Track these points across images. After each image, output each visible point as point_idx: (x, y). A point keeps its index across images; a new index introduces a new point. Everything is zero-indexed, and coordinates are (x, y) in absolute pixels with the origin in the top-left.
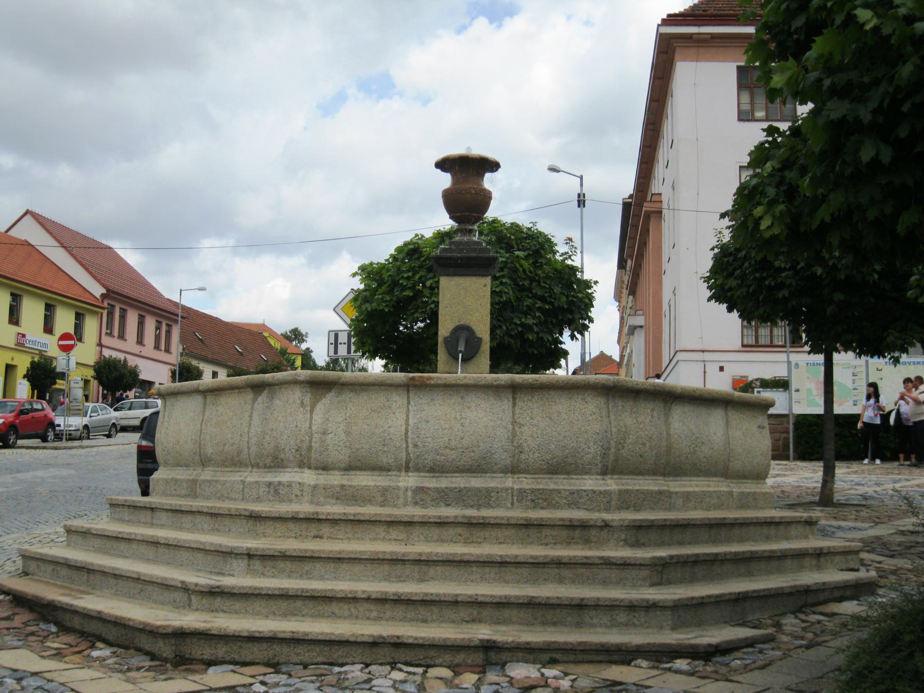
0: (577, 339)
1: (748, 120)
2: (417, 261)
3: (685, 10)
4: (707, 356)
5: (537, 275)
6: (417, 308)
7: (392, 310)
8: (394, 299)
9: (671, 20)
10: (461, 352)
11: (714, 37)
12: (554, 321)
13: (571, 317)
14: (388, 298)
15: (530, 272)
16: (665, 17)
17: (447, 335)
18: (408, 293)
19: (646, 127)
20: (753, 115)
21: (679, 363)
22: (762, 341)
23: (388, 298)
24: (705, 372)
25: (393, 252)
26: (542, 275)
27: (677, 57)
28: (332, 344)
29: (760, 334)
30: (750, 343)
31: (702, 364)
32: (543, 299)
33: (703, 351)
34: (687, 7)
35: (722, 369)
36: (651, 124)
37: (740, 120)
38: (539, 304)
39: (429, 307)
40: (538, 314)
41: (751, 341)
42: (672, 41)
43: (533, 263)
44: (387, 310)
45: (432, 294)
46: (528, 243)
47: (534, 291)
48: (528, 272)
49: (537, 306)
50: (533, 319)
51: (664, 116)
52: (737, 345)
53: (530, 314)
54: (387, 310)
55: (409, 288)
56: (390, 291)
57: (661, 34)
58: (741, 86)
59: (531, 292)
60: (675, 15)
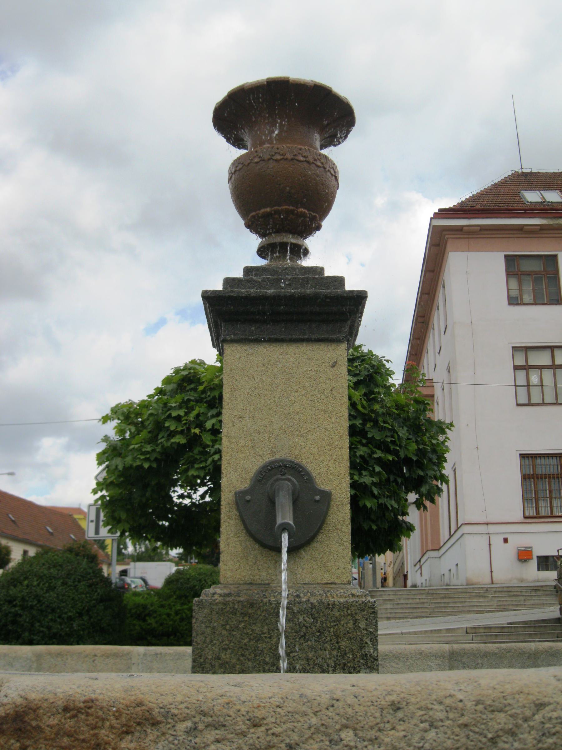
0: (425, 508)
1: (518, 304)
2: (192, 393)
3: (454, 206)
4: (492, 529)
5: (372, 411)
6: (191, 463)
7: (155, 465)
8: (159, 449)
9: (442, 213)
10: (285, 527)
11: (484, 229)
12: (399, 480)
13: (422, 473)
14: (149, 448)
15: (363, 407)
16: (437, 211)
17: (245, 486)
18: (180, 439)
19: (416, 320)
20: (522, 299)
21: (465, 536)
22: (543, 513)
23: (149, 448)
24: (490, 544)
25: (160, 385)
26: (381, 411)
27: (449, 246)
28: (92, 521)
29: (540, 505)
30: (531, 515)
31: (487, 536)
32: (383, 446)
33: (487, 524)
34: (456, 204)
35: (506, 540)
36: (421, 317)
37: (510, 304)
38: (378, 454)
39: (210, 460)
40: (378, 469)
41: (532, 512)
42: (444, 233)
43: (365, 394)
44: (146, 466)
45: (214, 442)
46: (356, 367)
47: (369, 435)
48: (359, 407)
49: (376, 456)
50: (371, 476)
51: (435, 306)
52: (519, 516)
53: (366, 469)
54: (146, 466)
55: (182, 432)
56: (153, 440)
57: (434, 226)
58: (509, 274)
59: (365, 437)
60: (445, 210)
